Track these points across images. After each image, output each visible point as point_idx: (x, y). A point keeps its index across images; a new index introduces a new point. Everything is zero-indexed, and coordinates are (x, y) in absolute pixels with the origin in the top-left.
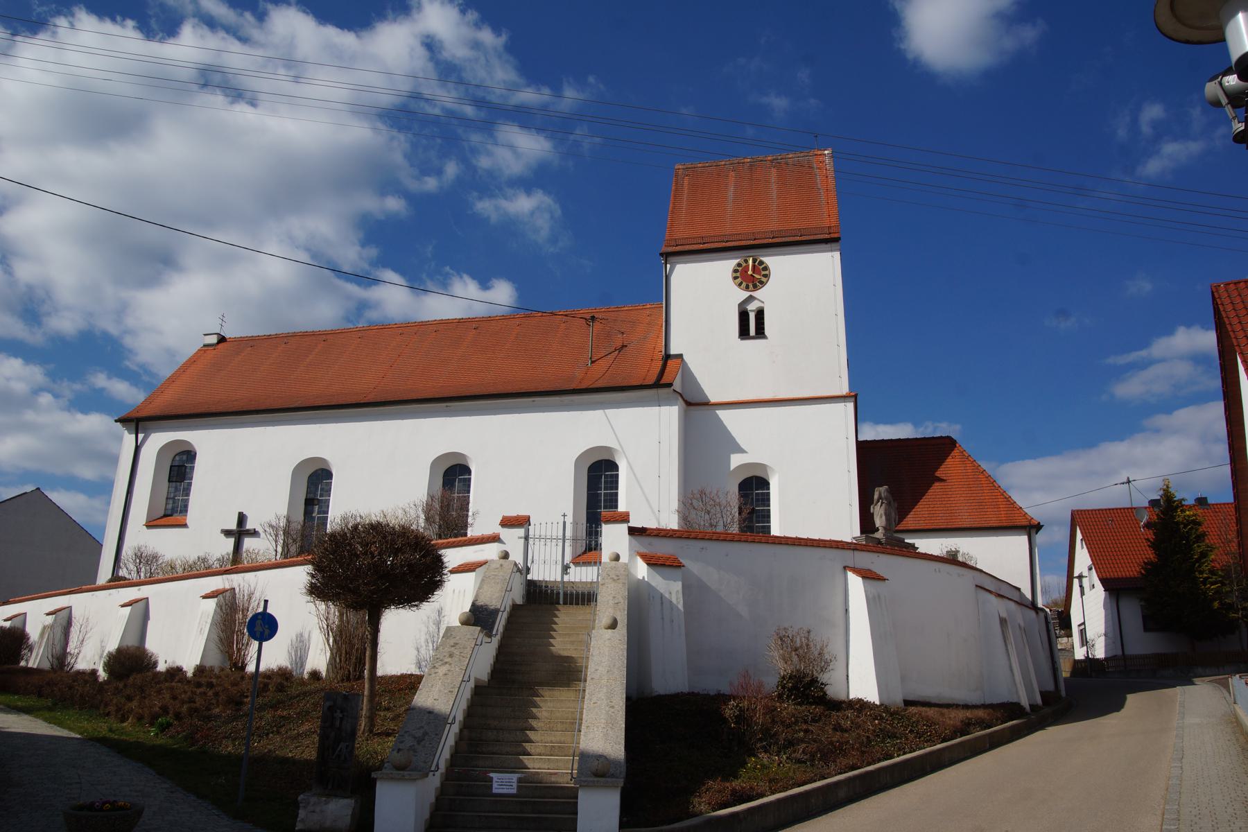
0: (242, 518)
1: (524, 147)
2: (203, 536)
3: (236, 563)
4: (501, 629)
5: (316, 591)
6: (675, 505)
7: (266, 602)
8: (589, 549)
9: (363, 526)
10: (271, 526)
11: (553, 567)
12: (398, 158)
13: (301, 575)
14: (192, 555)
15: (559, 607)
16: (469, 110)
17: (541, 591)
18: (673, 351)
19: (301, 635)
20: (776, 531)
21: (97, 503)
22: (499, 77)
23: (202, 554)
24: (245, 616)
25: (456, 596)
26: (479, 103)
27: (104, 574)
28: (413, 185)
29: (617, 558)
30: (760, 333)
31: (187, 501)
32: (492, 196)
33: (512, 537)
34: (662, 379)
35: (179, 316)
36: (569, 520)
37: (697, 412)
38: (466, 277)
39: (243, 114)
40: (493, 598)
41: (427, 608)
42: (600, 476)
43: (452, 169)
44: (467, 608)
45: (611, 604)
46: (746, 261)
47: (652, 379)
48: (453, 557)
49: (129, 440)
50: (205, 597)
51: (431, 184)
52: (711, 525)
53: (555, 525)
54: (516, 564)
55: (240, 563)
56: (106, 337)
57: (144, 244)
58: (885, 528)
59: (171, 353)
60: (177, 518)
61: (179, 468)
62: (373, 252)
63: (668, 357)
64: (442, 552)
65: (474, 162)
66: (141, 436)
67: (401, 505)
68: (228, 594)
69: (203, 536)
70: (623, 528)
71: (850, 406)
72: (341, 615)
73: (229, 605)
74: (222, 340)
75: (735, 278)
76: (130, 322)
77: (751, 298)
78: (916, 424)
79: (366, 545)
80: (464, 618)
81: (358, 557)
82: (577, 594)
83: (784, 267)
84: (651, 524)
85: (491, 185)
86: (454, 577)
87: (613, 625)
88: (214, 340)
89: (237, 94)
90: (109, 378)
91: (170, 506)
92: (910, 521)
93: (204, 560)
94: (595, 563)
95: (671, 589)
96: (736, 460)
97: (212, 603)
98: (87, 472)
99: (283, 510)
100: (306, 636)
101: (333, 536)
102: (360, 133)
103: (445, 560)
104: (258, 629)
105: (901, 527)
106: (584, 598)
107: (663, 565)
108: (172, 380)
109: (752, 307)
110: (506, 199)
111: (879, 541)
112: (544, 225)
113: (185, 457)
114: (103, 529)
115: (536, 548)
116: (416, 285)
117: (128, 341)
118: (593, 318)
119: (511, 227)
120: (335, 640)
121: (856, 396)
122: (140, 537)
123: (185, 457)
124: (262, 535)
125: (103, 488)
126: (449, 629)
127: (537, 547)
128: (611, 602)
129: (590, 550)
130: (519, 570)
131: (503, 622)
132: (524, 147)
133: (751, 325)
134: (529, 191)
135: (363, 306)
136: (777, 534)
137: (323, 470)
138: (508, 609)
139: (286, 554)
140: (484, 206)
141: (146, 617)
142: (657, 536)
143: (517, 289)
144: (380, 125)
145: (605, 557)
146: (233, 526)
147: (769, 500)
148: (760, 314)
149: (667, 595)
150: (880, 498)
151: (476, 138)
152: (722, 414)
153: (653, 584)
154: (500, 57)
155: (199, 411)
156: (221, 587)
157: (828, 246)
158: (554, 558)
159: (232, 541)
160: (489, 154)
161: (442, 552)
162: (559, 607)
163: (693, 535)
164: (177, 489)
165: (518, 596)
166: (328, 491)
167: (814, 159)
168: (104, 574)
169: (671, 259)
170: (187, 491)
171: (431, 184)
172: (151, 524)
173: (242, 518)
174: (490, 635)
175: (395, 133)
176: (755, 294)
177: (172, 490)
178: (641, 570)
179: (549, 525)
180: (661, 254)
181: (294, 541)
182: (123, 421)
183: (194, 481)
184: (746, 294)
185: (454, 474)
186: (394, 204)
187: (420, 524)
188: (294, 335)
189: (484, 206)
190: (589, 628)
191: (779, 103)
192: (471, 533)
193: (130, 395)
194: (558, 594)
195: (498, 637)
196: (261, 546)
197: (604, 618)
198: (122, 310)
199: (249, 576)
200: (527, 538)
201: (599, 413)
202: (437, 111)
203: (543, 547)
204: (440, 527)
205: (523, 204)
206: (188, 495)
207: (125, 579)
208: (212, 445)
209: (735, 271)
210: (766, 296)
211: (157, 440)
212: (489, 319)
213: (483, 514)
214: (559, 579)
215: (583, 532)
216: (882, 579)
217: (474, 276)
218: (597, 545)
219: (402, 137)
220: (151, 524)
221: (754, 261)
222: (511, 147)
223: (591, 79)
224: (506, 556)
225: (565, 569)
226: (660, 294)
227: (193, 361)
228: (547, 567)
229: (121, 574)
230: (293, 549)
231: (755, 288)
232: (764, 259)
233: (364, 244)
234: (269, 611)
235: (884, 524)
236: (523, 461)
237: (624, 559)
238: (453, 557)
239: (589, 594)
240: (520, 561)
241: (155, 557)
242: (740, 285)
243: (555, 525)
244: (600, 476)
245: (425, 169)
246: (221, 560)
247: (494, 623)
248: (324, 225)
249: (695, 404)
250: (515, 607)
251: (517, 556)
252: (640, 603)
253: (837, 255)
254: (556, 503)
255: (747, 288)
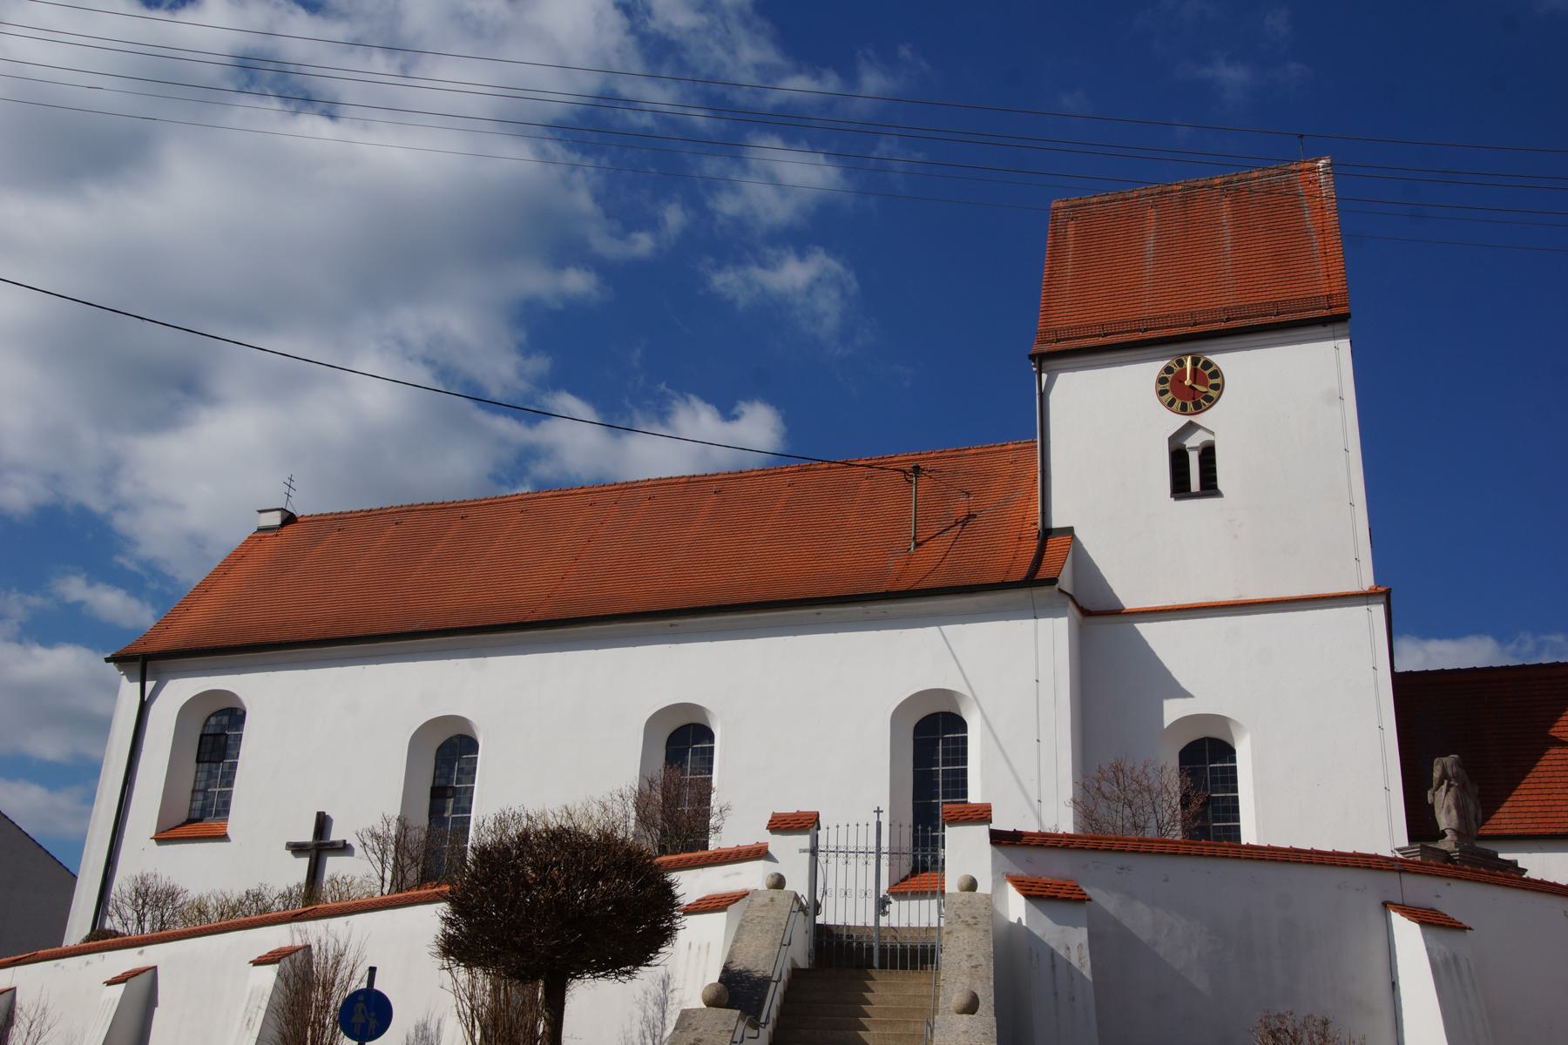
0: (323, 823)
1: (794, 175)
2: (252, 853)
3: (312, 901)
4: (774, 1014)
5: (454, 949)
6: (1067, 791)
7: (372, 970)
8: (919, 866)
9: (537, 834)
10: (375, 836)
11: (861, 902)
12: (583, 201)
13: (427, 921)
14: (236, 889)
15: (874, 973)
16: (700, 119)
17: (840, 944)
18: (1057, 522)
19: (425, 1027)
20: (1250, 833)
21: (65, 800)
22: (748, 57)
23: (253, 887)
24: (328, 996)
25: (696, 955)
26: (718, 105)
27: (78, 927)
28: (605, 245)
29: (972, 885)
30: (1210, 487)
31: (229, 794)
32: (739, 262)
33: (790, 851)
34: (1039, 570)
35: (216, 476)
36: (885, 819)
37: (1104, 627)
38: (694, 399)
39: (312, 129)
40: (761, 958)
41: (646, 977)
42: (934, 742)
43: (674, 217)
44: (714, 976)
45: (964, 969)
46: (1181, 363)
47: (1020, 573)
48: (690, 885)
49: (129, 692)
50: (257, 963)
51: (643, 244)
52: (1135, 826)
53: (862, 827)
54: (797, 898)
55: (318, 901)
56: (83, 512)
57: (149, 355)
58: (1457, 832)
59: (197, 541)
60: (211, 824)
61: (216, 739)
62: (540, 364)
63: (1047, 532)
64: (673, 876)
65: (710, 204)
66: (150, 685)
67: (597, 797)
68: (299, 955)
69: (252, 853)
70: (982, 832)
71: (1379, 611)
72: (496, 989)
73: (300, 979)
74: (289, 519)
75: (1161, 393)
76: (126, 489)
77: (1190, 428)
78: (1502, 637)
79: (541, 867)
80: (710, 995)
81: (528, 888)
82: (904, 949)
83: (1243, 369)
84: (1030, 826)
85: (742, 243)
86: (691, 921)
87: (971, 1007)
88: (274, 519)
89: (299, 93)
90: (90, 584)
91: (198, 804)
92: (1504, 819)
93: (258, 897)
94: (933, 894)
95: (1070, 941)
96: (1173, 710)
97: (270, 973)
98: (48, 746)
99: (395, 810)
100: (433, 1028)
101: (483, 853)
102: (514, 161)
103: (678, 892)
104: (358, 1019)
105: (1486, 830)
106: (917, 956)
107: (1054, 898)
108: (205, 587)
109: (1194, 442)
110: (763, 265)
111: (1446, 856)
112: (828, 305)
113: (225, 720)
114: (78, 846)
115: (834, 872)
116: (616, 421)
117: (121, 522)
118: (917, 469)
119: (773, 313)
120: (484, 1034)
121: (1388, 594)
122: (143, 858)
123: (225, 720)
124: (358, 850)
125: (85, 773)
126: (685, 1015)
127: (831, 867)
128: (965, 965)
129: (925, 870)
130: (802, 909)
131: (777, 1001)
132: (794, 175)
133: (1193, 473)
134: (802, 255)
135: (529, 454)
136: (1254, 842)
137: (462, 737)
138: (785, 977)
139: (399, 884)
140: (725, 281)
141: (150, 1001)
142: (1040, 846)
143: (785, 420)
144: (555, 149)
145: (952, 884)
146: (307, 836)
147: (1235, 780)
148: (1208, 453)
149: (1062, 952)
150: (1445, 776)
151: (712, 166)
152: (1146, 629)
153: (1038, 932)
154: (746, 23)
155: (250, 640)
156: (286, 942)
157: (1329, 328)
158: (861, 886)
159: (304, 863)
160: (735, 190)
161: (673, 876)
162: (874, 973)
163: (1104, 844)
164: (210, 775)
165: (800, 952)
166: (470, 773)
167: (1298, 177)
168: (78, 927)
169: (1047, 364)
170: (229, 778)
171: (643, 244)
172: (165, 836)
173: (323, 823)
174: (755, 1024)
175: (575, 158)
176: (1197, 419)
177: (204, 776)
178: (1015, 907)
179: (853, 828)
180: (1032, 357)
181: (414, 860)
182: (119, 659)
183: (240, 761)
184: (1182, 420)
185: (685, 742)
186: (577, 282)
187: (627, 825)
188: (411, 509)
189: (725, 281)
190: (927, 1013)
191: (1232, 76)
192: (715, 843)
193: (130, 613)
194: (870, 949)
195: (770, 1027)
196: (356, 871)
197: (954, 995)
198: (112, 469)
199: (337, 923)
200: (814, 851)
201: (932, 631)
202: (646, 120)
203: (841, 867)
204: (664, 832)
205: (793, 275)
206: (230, 784)
207: (115, 934)
208: (261, 691)
209: (1162, 381)
210: (1216, 422)
211: (179, 691)
212: (739, 476)
213: (737, 811)
214: (871, 923)
215: (907, 842)
216: (1464, 928)
217: (708, 399)
218: (935, 861)
219: (589, 162)
220: (165, 836)
221: (1195, 362)
222: (774, 181)
223: (904, 51)
224: (779, 883)
225: (882, 906)
226: (1030, 425)
227: (238, 556)
228: (850, 901)
229: (108, 924)
230: (412, 875)
231: (1199, 408)
232: (1213, 358)
233: (526, 351)
234: (377, 986)
235: (1454, 824)
236: (801, 720)
237: (984, 887)
238: (690, 885)
239: (924, 949)
240: (803, 891)
241: (171, 894)
242: (1170, 404)
243: (862, 827)
244: (934, 742)
245: (629, 219)
246: (287, 897)
247: (762, 1001)
248: (463, 321)
249: (1098, 613)
250: (796, 973)
251: (798, 884)
252: (1013, 958)
253: (1345, 345)
254: (861, 791)
255: (1183, 410)
